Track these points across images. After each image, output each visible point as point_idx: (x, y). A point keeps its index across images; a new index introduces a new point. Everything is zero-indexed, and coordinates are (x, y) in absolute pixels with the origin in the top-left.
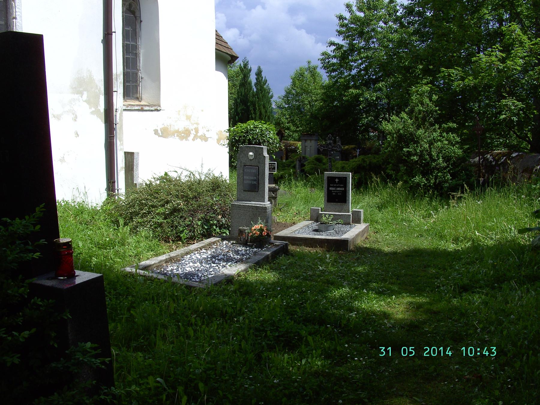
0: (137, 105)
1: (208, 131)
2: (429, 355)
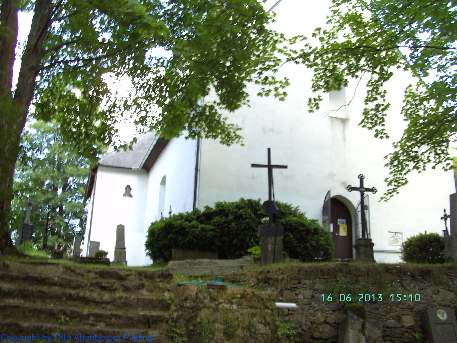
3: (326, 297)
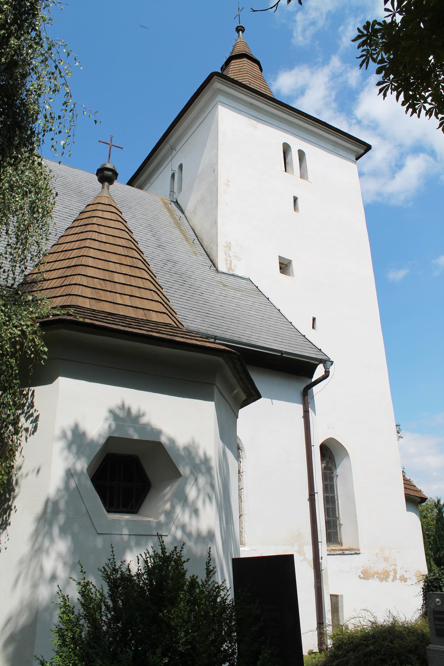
0: (339, 550)
1: (407, 571)
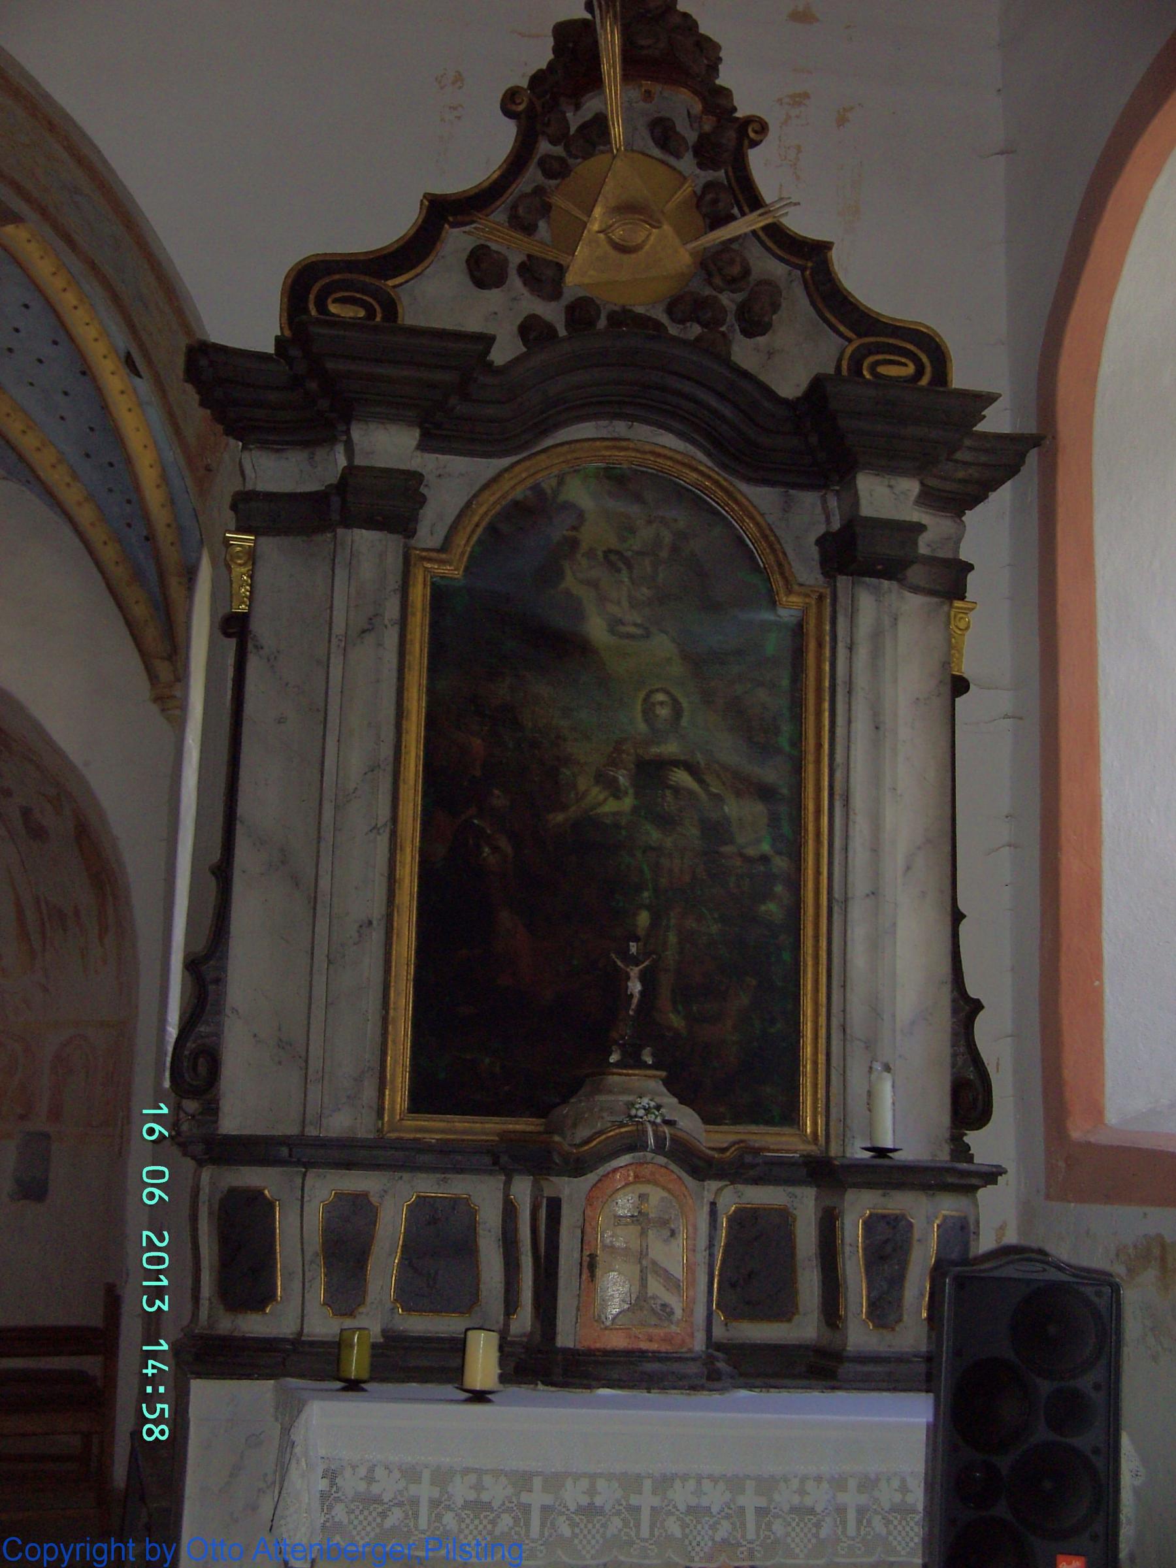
2: (144, 1244)
3: (157, 1119)
